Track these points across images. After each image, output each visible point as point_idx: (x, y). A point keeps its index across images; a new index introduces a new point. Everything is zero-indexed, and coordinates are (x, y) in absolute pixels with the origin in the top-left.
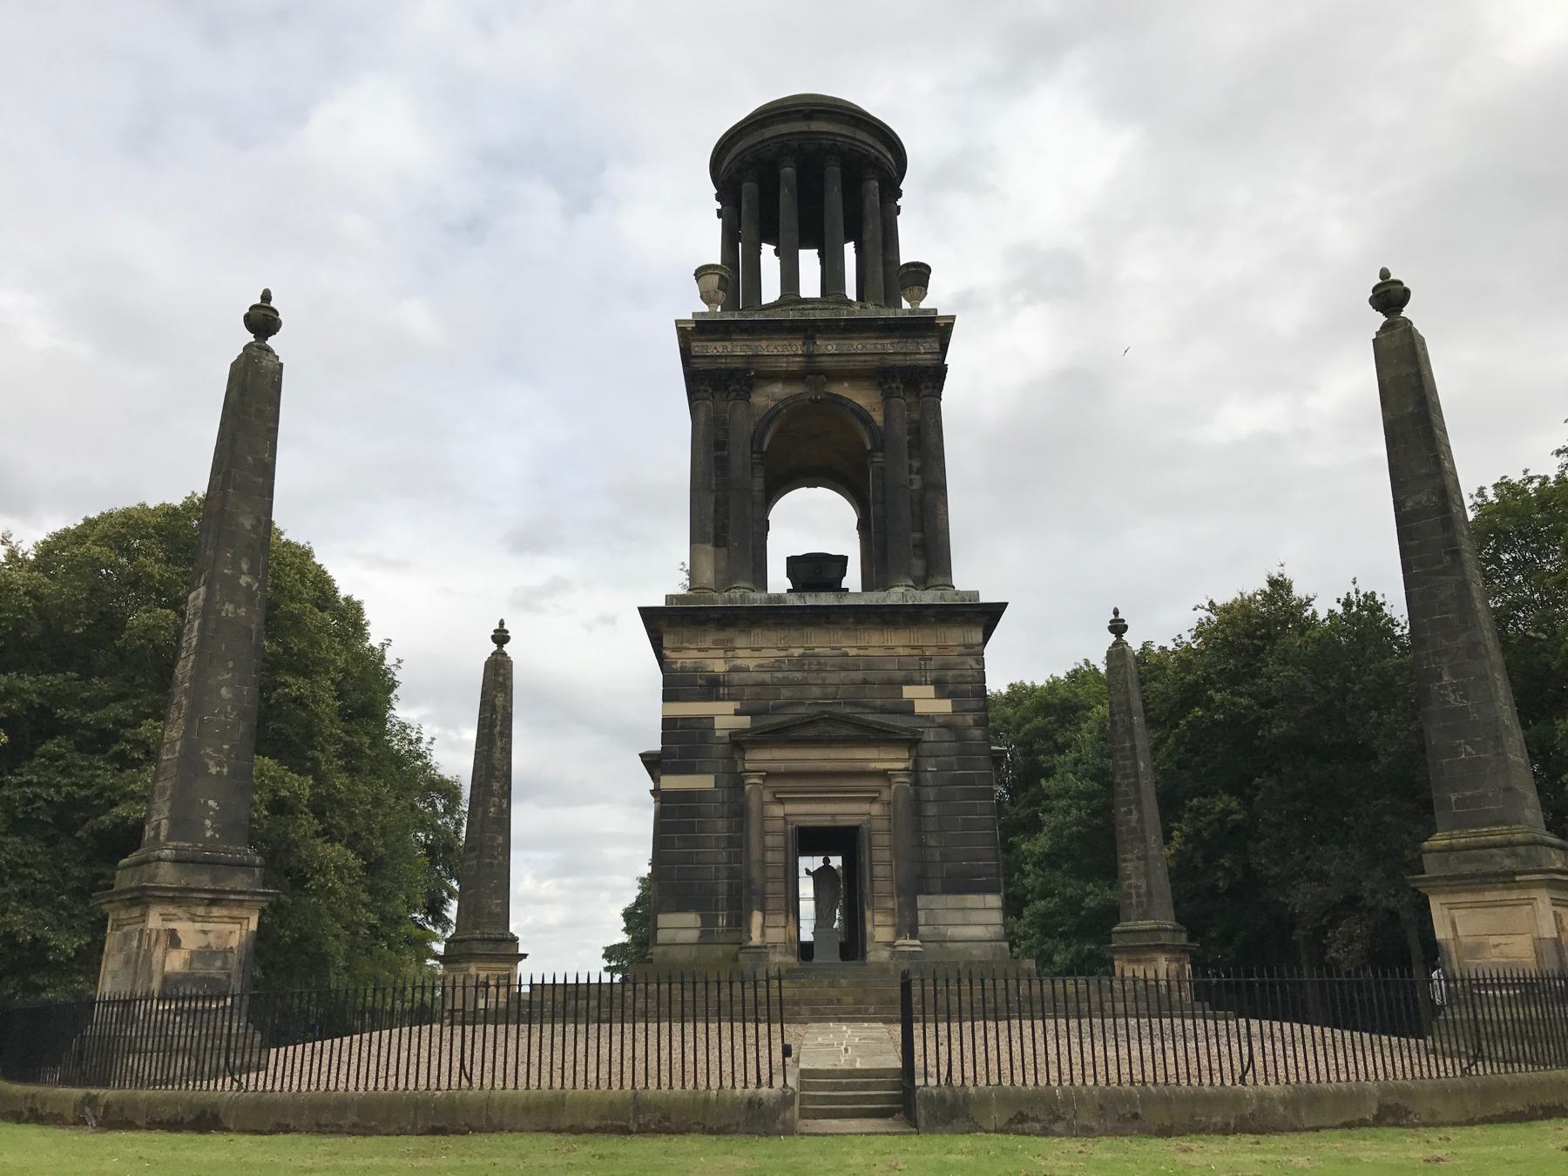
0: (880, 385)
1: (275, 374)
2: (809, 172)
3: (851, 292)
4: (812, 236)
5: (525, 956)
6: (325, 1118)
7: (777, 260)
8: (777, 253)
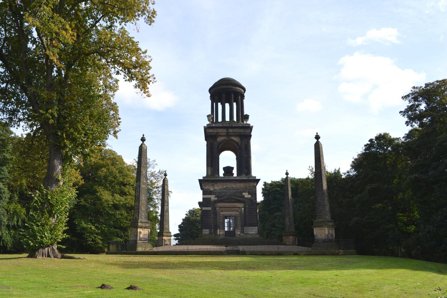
3: (235, 119)
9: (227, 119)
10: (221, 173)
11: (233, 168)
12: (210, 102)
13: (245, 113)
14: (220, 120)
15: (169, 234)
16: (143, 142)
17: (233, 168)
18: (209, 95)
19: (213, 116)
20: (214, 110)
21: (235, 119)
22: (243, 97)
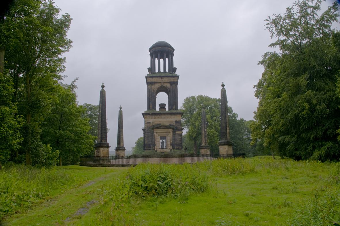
0: (170, 84)
1: (105, 92)
2: (162, 51)
3: (167, 71)
4: (162, 57)
5: (110, 147)
6: (117, 166)
7: (158, 60)
8: (158, 59)
9: (162, 70)
10: (158, 108)
11: (165, 105)
12: (150, 58)
13: (174, 66)
14: (157, 71)
15: (123, 149)
16: (223, 87)
17: (165, 105)
18: (149, 53)
19: (151, 70)
20: (153, 64)
21: (167, 71)
22: (172, 55)
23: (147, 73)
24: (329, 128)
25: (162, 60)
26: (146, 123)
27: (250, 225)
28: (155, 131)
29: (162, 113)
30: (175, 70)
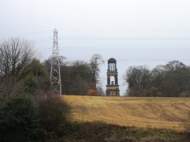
3: (114, 70)
9: (112, 70)
14: (110, 70)
21: (114, 70)
23: (107, 71)
24: (164, 133)
25: (112, 64)
26: (107, 89)
27: (23, 141)
28: (110, 92)
29: (113, 85)
30: (117, 70)
